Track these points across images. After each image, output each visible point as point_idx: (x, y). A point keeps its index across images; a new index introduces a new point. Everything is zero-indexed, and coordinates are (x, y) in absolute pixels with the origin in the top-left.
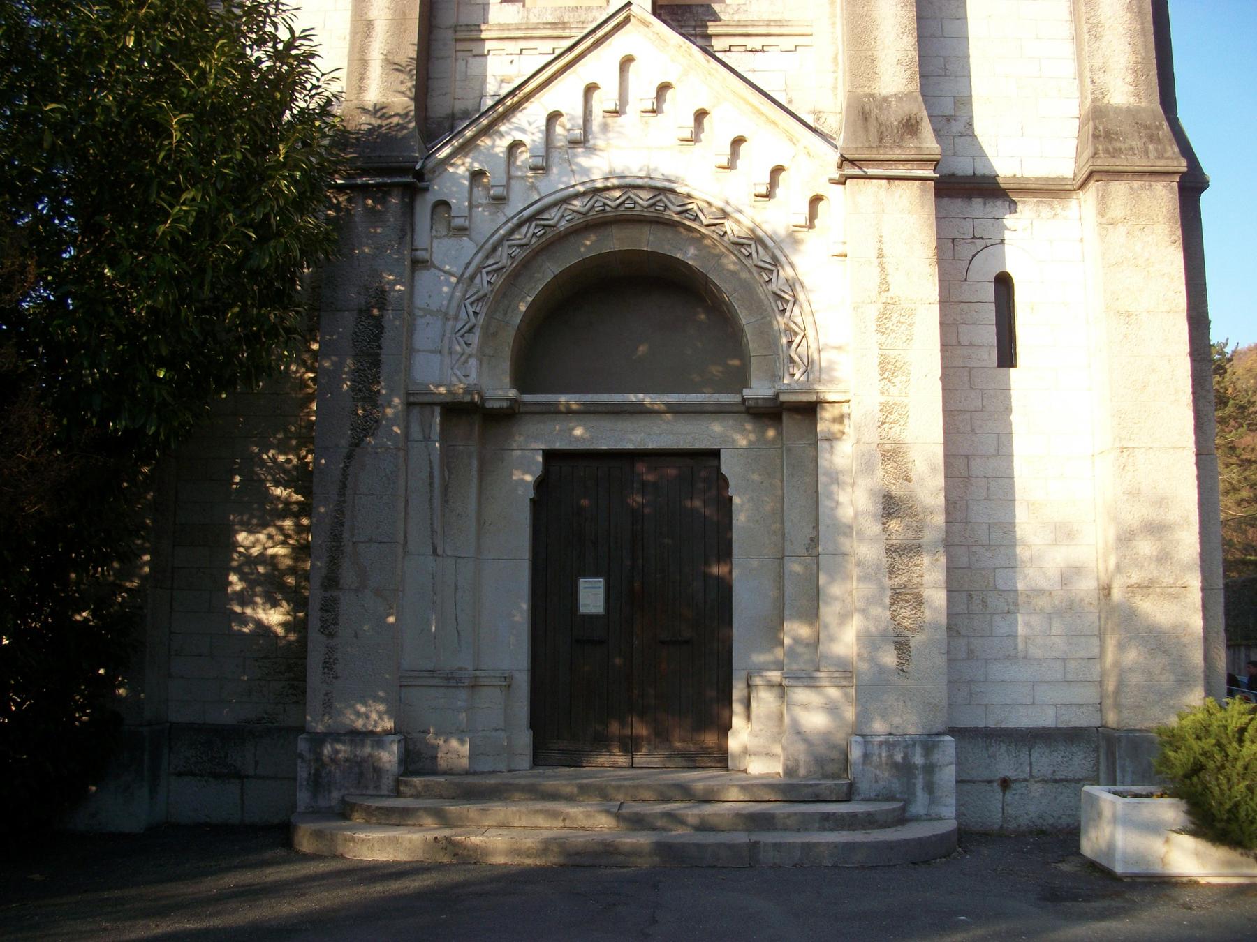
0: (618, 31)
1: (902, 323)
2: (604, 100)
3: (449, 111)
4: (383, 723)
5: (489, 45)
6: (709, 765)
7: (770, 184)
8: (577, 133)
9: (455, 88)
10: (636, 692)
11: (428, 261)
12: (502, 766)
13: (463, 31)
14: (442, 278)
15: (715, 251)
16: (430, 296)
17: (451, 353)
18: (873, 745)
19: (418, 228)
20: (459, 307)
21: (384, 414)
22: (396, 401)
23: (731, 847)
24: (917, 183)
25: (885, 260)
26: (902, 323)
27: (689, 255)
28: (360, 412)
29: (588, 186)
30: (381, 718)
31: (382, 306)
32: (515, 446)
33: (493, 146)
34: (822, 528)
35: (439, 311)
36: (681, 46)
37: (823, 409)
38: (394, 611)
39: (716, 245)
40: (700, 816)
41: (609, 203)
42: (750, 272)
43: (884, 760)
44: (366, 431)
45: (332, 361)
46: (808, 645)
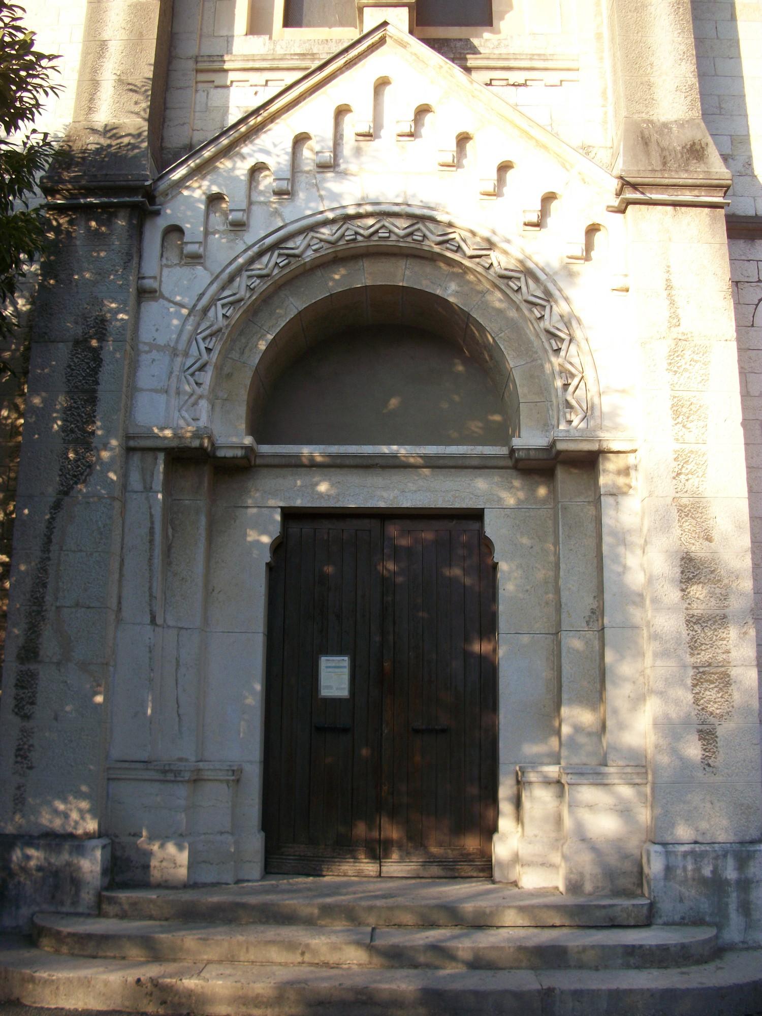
0: (372, 52)
1: (696, 361)
2: (352, 125)
3: (187, 141)
4: (85, 824)
5: (232, 76)
6: (469, 874)
7: (541, 211)
8: (327, 155)
9: (194, 119)
10: (385, 788)
11: (155, 291)
12: (229, 877)
13: (204, 61)
14: (172, 310)
15: (479, 288)
16: (157, 330)
17: (178, 393)
18: (676, 856)
19: (146, 255)
20: (189, 343)
21: (99, 458)
22: (114, 442)
23: (518, 995)
24: (706, 210)
25: (673, 293)
26: (696, 361)
27: (449, 292)
28: (71, 455)
29: (339, 212)
30: (83, 818)
31: (102, 338)
32: (250, 502)
33: (234, 169)
34: (607, 596)
35: (167, 346)
36: (441, 67)
37: (608, 459)
38: (102, 689)
39: (480, 281)
40: (476, 952)
41: (362, 231)
42: (518, 309)
43: (690, 874)
44: (78, 477)
45: (42, 397)
46: (589, 734)
